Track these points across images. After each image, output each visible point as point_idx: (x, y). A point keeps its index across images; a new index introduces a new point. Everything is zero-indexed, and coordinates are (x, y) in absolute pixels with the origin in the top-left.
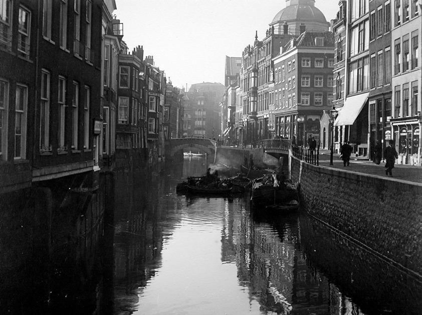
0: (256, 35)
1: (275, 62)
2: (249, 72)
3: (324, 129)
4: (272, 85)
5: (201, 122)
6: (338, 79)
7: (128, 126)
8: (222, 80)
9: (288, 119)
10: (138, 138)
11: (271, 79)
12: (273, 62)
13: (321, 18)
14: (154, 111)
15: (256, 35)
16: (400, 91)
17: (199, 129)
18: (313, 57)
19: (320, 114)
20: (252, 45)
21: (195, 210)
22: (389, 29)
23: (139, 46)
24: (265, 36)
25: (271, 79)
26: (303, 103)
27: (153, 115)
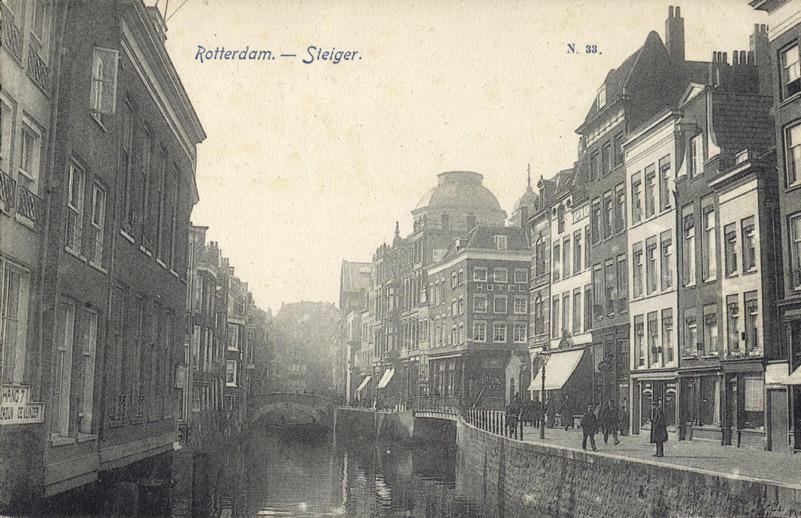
0: (397, 228)
1: (430, 273)
2: (385, 288)
3: (512, 379)
4: (425, 310)
5: (299, 366)
6: (538, 301)
7: (710, 325)
8: (334, 298)
9: (452, 367)
10: (210, 395)
11: (423, 299)
12: (425, 272)
13: (495, 210)
14: (236, 349)
15: (397, 228)
16: (643, 324)
17: (294, 377)
18: (491, 266)
19: (506, 357)
20: (390, 243)
21: (34, 293)
22: (620, 223)
23: (212, 242)
24: (412, 231)
25: (423, 299)
26: (477, 339)
27: (232, 355)
